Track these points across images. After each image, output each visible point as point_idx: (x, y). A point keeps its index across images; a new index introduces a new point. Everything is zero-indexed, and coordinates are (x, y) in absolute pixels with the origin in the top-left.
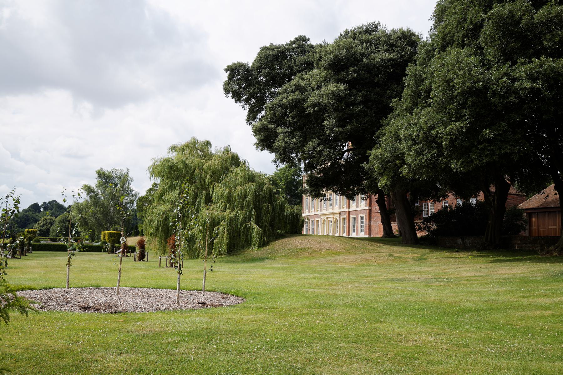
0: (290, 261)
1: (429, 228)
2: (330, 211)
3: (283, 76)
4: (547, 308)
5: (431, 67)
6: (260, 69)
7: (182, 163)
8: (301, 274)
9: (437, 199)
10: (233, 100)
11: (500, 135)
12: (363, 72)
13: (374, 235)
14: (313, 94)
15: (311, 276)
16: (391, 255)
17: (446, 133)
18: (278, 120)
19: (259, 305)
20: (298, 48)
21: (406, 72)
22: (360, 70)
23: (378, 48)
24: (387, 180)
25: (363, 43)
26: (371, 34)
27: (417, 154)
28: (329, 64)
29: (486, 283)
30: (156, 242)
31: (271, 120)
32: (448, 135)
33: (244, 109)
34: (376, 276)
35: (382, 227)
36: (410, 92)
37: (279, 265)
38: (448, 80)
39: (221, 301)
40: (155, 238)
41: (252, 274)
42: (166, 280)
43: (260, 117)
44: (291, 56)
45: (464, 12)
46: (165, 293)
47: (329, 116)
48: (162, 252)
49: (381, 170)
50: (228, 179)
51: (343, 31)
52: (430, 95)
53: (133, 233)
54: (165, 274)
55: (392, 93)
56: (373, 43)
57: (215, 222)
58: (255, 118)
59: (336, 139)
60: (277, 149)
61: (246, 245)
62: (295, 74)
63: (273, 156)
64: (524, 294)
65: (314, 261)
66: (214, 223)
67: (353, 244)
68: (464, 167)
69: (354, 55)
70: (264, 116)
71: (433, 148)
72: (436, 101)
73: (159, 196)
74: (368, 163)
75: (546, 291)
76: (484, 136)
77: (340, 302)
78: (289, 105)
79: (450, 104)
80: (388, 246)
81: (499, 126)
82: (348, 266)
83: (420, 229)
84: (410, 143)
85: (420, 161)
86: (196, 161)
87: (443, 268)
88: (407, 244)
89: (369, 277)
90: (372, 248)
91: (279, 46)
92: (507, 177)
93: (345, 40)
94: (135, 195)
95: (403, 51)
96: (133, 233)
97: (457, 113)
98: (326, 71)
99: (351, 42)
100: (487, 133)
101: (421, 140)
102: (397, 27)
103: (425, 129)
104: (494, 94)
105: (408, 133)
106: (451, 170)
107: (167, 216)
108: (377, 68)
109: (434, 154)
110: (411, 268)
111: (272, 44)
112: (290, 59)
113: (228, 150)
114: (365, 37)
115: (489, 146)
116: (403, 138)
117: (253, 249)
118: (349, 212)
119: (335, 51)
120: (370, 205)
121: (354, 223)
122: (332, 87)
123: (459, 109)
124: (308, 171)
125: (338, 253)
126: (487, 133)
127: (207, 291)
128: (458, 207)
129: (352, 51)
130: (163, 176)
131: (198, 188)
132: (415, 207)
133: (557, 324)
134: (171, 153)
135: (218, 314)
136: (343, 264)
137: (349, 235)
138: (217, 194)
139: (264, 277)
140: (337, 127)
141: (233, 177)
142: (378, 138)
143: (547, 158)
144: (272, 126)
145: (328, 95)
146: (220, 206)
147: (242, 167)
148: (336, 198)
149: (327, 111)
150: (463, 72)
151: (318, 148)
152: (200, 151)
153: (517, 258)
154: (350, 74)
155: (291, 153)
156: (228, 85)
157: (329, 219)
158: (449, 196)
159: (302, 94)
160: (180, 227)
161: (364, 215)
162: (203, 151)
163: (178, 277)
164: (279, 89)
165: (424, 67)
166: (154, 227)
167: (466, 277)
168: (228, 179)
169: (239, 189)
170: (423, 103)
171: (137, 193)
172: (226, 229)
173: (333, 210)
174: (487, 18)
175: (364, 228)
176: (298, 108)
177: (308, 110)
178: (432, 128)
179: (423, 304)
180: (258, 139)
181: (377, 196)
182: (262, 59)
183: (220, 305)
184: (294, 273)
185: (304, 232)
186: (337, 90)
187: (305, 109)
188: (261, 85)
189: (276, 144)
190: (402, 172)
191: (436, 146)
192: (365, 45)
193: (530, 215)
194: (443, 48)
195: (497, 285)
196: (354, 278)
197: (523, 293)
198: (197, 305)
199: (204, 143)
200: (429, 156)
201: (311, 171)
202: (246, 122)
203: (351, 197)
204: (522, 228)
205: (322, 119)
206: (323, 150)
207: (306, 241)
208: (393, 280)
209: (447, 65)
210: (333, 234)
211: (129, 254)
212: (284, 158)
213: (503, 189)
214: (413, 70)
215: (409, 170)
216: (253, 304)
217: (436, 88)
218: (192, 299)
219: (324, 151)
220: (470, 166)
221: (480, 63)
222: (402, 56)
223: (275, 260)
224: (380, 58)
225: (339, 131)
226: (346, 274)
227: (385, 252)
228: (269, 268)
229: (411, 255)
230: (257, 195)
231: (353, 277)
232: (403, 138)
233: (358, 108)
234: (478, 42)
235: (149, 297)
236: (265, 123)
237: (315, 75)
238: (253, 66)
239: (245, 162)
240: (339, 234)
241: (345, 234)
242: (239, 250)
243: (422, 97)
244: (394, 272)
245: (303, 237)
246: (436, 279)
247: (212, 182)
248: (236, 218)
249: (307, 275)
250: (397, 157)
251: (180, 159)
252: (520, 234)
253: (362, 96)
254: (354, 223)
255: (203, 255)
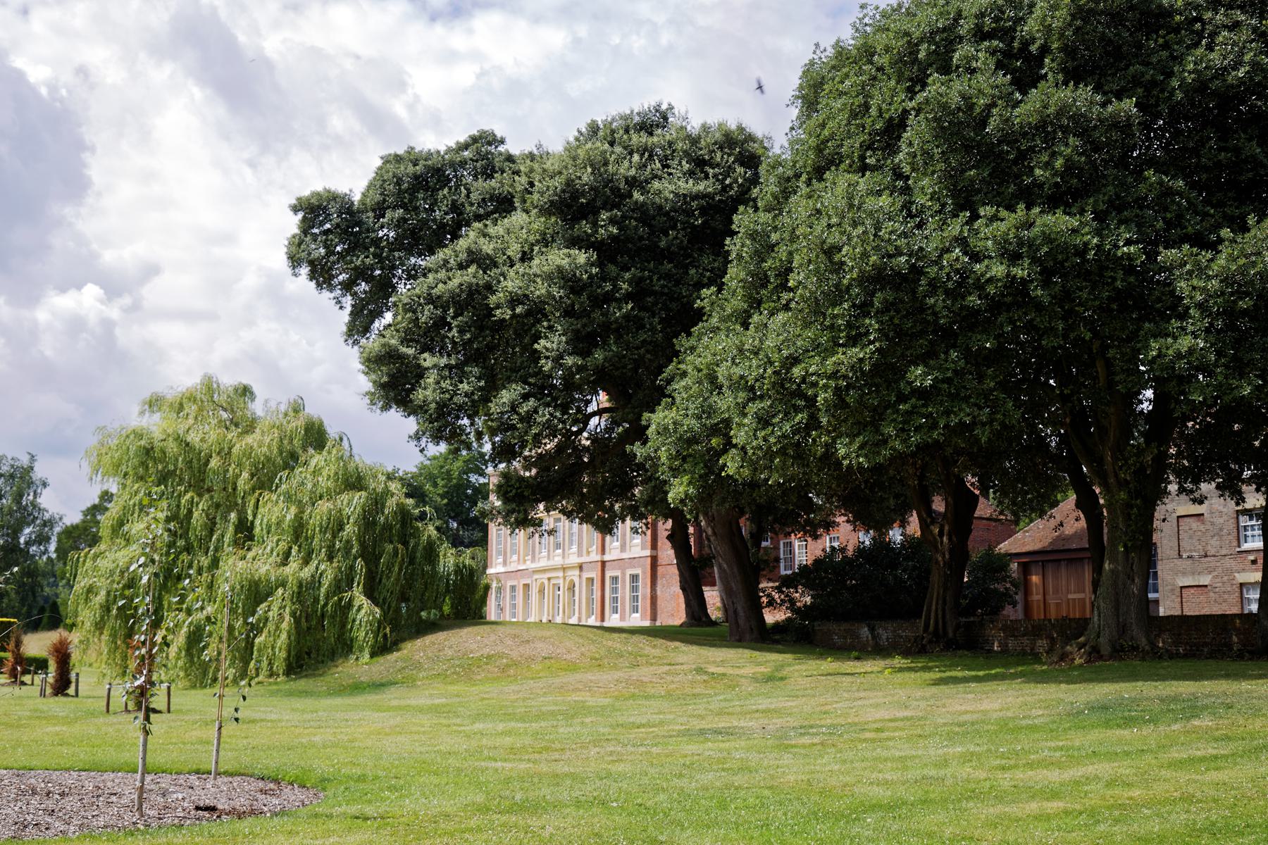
0: (451, 688)
1: (792, 602)
2: (558, 560)
3: (439, 228)
4: (1055, 795)
5: (791, 217)
6: (380, 210)
7: (176, 440)
8: (474, 723)
9: (812, 531)
10: (313, 284)
11: (948, 381)
12: (634, 223)
13: (665, 620)
14: (512, 273)
15: (501, 727)
16: (700, 670)
17: (825, 373)
18: (428, 337)
19: (354, 809)
20: (477, 161)
21: (734, 227)
22: (624, 217)
23: (668, 166)
24: (690, 483)
25: (631, 153)
26: (651, 134)
27: (759, 423)
28: (552, 202)
29: (920, 736)
30: (103, 644)
31: (406, 335)
32: (829, 378)
33: (341, 308)
34: (661, 723)
35: (682, 599)
36: (742, 275)
37: (422, 702)
38: (830, 248)
39: (257, 800)
40: (101, 634)
41: (349, 726)
42: (119, 746)
43: (381, 328)
44: (459, 179)
45: (863, 91)
46: (109, 784)
47: (550, 328)
48: (119, 670)
49: (676, 460)
50: (295, 482)
51: (585, 125)
52: (787, 281)
53: (45, 620)
54: (118, 731)
55: (701, 274)
56: (656, 155)
57: (256, 593)
58: (366, 330)
59: (569, 385)
60: (421, 407)
61: (340, 650)
62: (468, 224)
63: (411, 424)
64: (1004, 762)
65: (513, 687)
66: (257, 592)
67: (610, 643)
68: (866, 456)
69: (611, 181)
70: (390, 325)
71: (797, 410)
72: (801, 295)
73: (112, 525)
74: (645, 443)
75: (1055, 751)
76: (912, 382)
77: (565, 793)
78: (453, 298)
79: (834, 305)
80: (695, 648)
81: (946, 361)
82: (594, 699)
83: (771, 603)
84: (742, 396)
85: (765, 439)
86: (213, 436)
87: (822, 700)
88: (740, 640)
89: (643, 726)
90: (657, 652)
91: (430, 154)
92: (970, 479)
93: (589, 145)
94: (49, 523)
95: (727, 175)
96: (45, 620)
97: (849, 325)
98: (543, 219)
99: (606, 152)
100: (919, 376)
101: (768, 390)
102: (713, 119)
103: (776, 364)
104: (934, 285)
105: (738, 371)
106: (838, 464)
107: (133, 579)
108: (667, 214)
109: (798, 423)
110: (748, 702)
111: (412, 148)
112: (457, 187)
113: (297, 409)
114: (637, 139)
115: (923, 406)
116: (726, 383)
117: (357, 659)
118: (603, 563)
119: (564, 171)
120: (654, 546)
121: (615, 590)
122: (559, 257)
123: (854, 316)
124: (500, 462)
125: (572, 667)
126: (919, 376)
127: (228, 774)
128: (861, 551)
129: (606, 171)
130: (126, 474)
131: (218, 506)
132: (762, 551)
133: (1074, 834)
134: (147, 414)
135: (245, 836)
136: (583, 693)
137: (603, 620)
138: (265, 520)
139: (379, 734)
140: (570, 354)
141: (308, 476)
142: (669, 381)
143: (1059, 435)
144: (411, 351)
145: (548, 277)
146: (272, 551)
147: (329, 453)
148: (570, 529)
149: (545, 316)
150: (860, 230)
151: (524, 405)
152: (225, 410)
153: (993, 672)
154: (602, 226)
155: (458, 418)
156: (299, 245)
157: (553, 582)
158: (838, 525)
159: (485, 273)
160: (148, 610)
161: (638, 571)
162: (232, 411)
163: (141, 740)
164: (428, 258)
165: (775, 216)
166: (97, 606)
167: (875, 722)
168: (295, 482)
169: (324, 506)
170: (774, 301)
171: (57, 517)
172: (288, 610)
173: (563, 557)
174: (913, 109)
175: (639, 604)
176: (474, 307)
177: (498, 312)
178: (794, 360)
179: (766, 793)
180: (374, 382)
181: (670, 523)
182: (385, 185)
183: (253, 812)
184: (458, 721)
185: (491, 611)
186: (570, 265)
187: (492, 309)
188: (383, 248)
189: (419, 395)
190: (725, 465)
191: (803, 403)
192: (636, 158)
193: (1026, 569)
194: (819, 172)
195: (945, 740)
196: (606, 730)
197: (1002, 758)
198: (193, 812)
199: (236, 390)
200: (787, 427)
201: (509, 462)
202: (343, 339)
203: (606, 527)
204: (1006, 598)
205: (535, 334)
206: (536, 411)
207: (493, 637)
208: (702, 732)
209: (827, 214)
210: (563, 618)
211: (27, 678)
212: (439, 430)
213: (963, 504)
214: (750, 222)
215: (743, 461)
216: (340, 806)
217: (801, 265)
218: (180, 797)
219: (538, 413)
220: (879, 453)
221: (901, 211)
222: (725, 189)
223: (414, 686)
224: (673, 192)
225: (575, 364)
226: (588, 720)
227: (688, 664)
228: (399, 708)
229: (749, 670)
230: (368, 520)
231: (605, 727)
232: (726, 383)
233: (620, 310)
234: (897, 160)
235: (62, 795)
236: (393, 342)
237: (518, 227)
238: (362, 202)
239: (341, 439)
240: (580, 619)
241: (593, 617)
242: (323, 662)
243: (770, 287)
244: (704, 712)
245: (485, 627)
246: (804, 730)
247: (253, 490)
248: (315, 582)
249: (490, 726)
250: (714, 430)
251: (170, 431)
252: (1005, 612)
253: (630, 282)
254: (615, 590)
255: (227, 678)
